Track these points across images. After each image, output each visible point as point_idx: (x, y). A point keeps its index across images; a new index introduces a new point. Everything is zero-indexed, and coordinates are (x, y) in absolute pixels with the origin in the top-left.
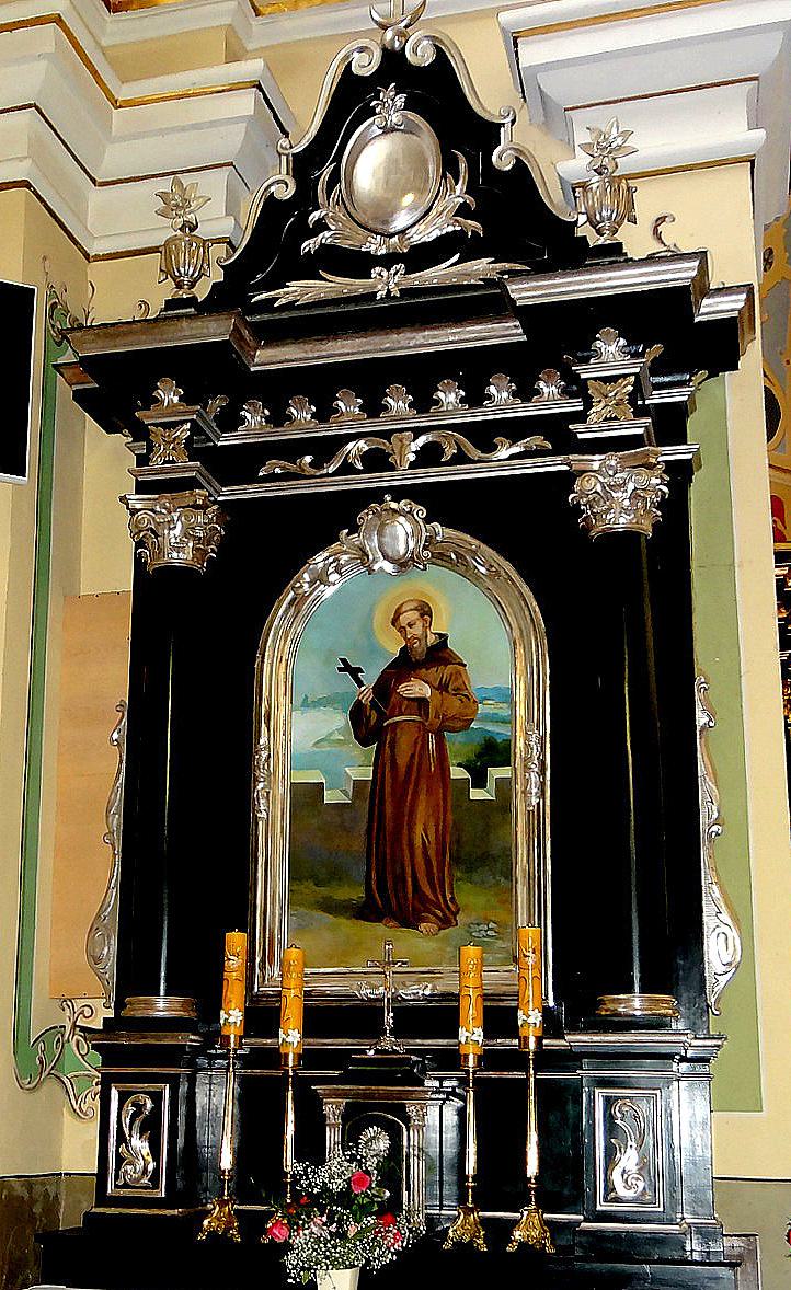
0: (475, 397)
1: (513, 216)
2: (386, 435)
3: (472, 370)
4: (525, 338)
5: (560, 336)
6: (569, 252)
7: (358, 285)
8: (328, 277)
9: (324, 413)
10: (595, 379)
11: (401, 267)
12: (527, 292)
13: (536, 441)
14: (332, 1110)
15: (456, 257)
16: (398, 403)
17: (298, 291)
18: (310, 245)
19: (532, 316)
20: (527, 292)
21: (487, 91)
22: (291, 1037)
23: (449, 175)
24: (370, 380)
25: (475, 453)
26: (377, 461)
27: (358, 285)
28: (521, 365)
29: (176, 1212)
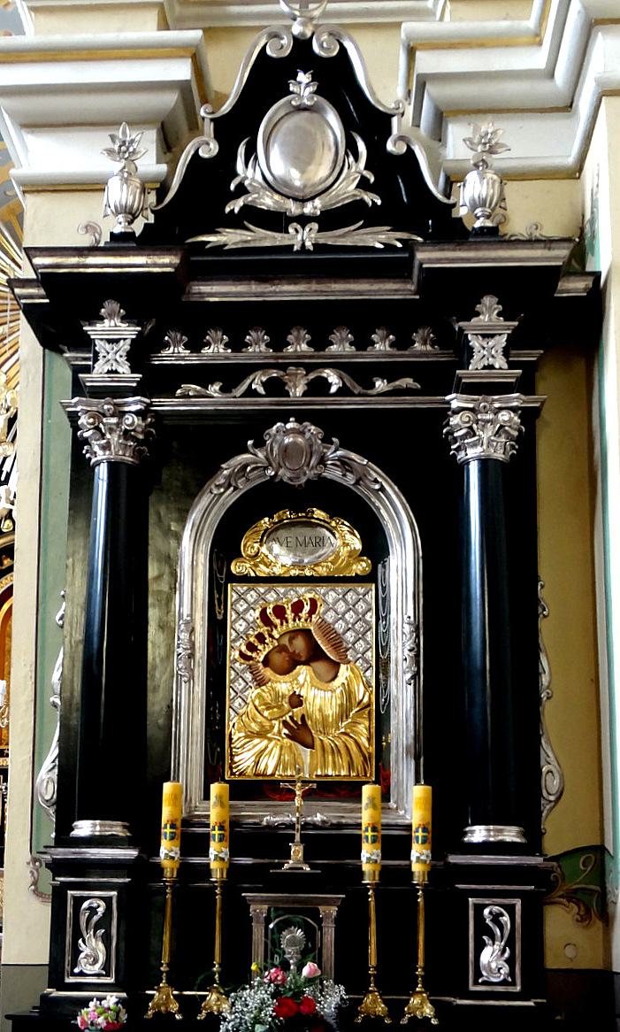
0: (362, 342)
1: (402, 192)
2: (283, 367)
3: (362, 319)
4: (47, 301)
5: (450, 297)
6: (450, 230)
7: (277, 239)
8: (251, 227)
9: (237, 344)
10: (102, 339)
11: (315, 226)
12: (429, 257)
13: (407, 382)
14: (258, 910)
15: (361, 223)
16: (300, 346)
17: (230, 238)
18: (236, 206)
19: (433, 278)
20: (429, 257)
21: (382, 81)
22: (217, 849)
23: (349, 153)
24: (278, 320)
25: (358, 389)
26: (275, 388)
27: (277, 239)
28: (398, 319)
29: (531, 1003)
